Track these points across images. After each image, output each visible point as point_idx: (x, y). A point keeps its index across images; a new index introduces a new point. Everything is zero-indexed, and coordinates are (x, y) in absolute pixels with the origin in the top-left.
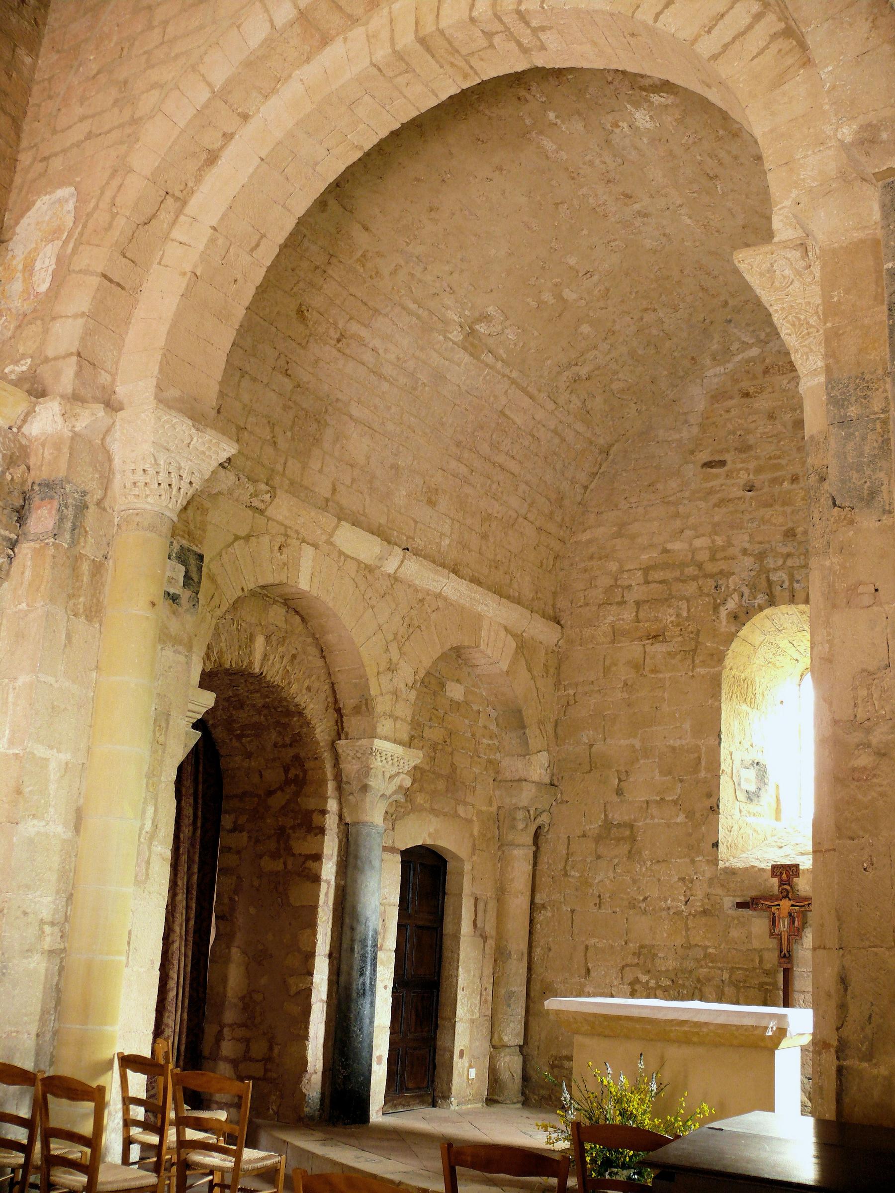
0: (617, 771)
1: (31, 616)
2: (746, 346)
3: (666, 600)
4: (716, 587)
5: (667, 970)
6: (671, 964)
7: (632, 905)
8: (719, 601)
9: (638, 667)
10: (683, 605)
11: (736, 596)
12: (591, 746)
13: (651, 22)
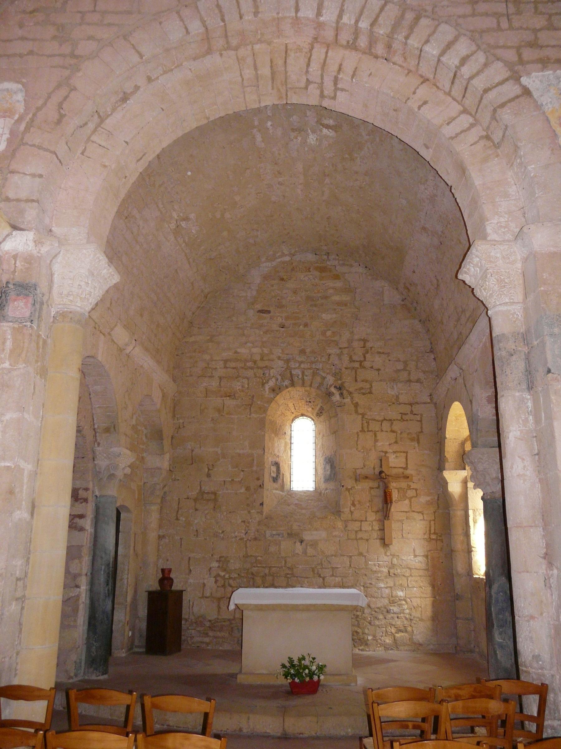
0: (207, 464)
1: (15, 373)
2: (283, 255)
3: (237, 378)
4: (264, 374)
5: (235, 569)
6: (237, 566)
7: (216, 535)
8: (264, 381)
9: (219, 411)
10: (245, 381)
11: (274, 380)
12: (192, 451)
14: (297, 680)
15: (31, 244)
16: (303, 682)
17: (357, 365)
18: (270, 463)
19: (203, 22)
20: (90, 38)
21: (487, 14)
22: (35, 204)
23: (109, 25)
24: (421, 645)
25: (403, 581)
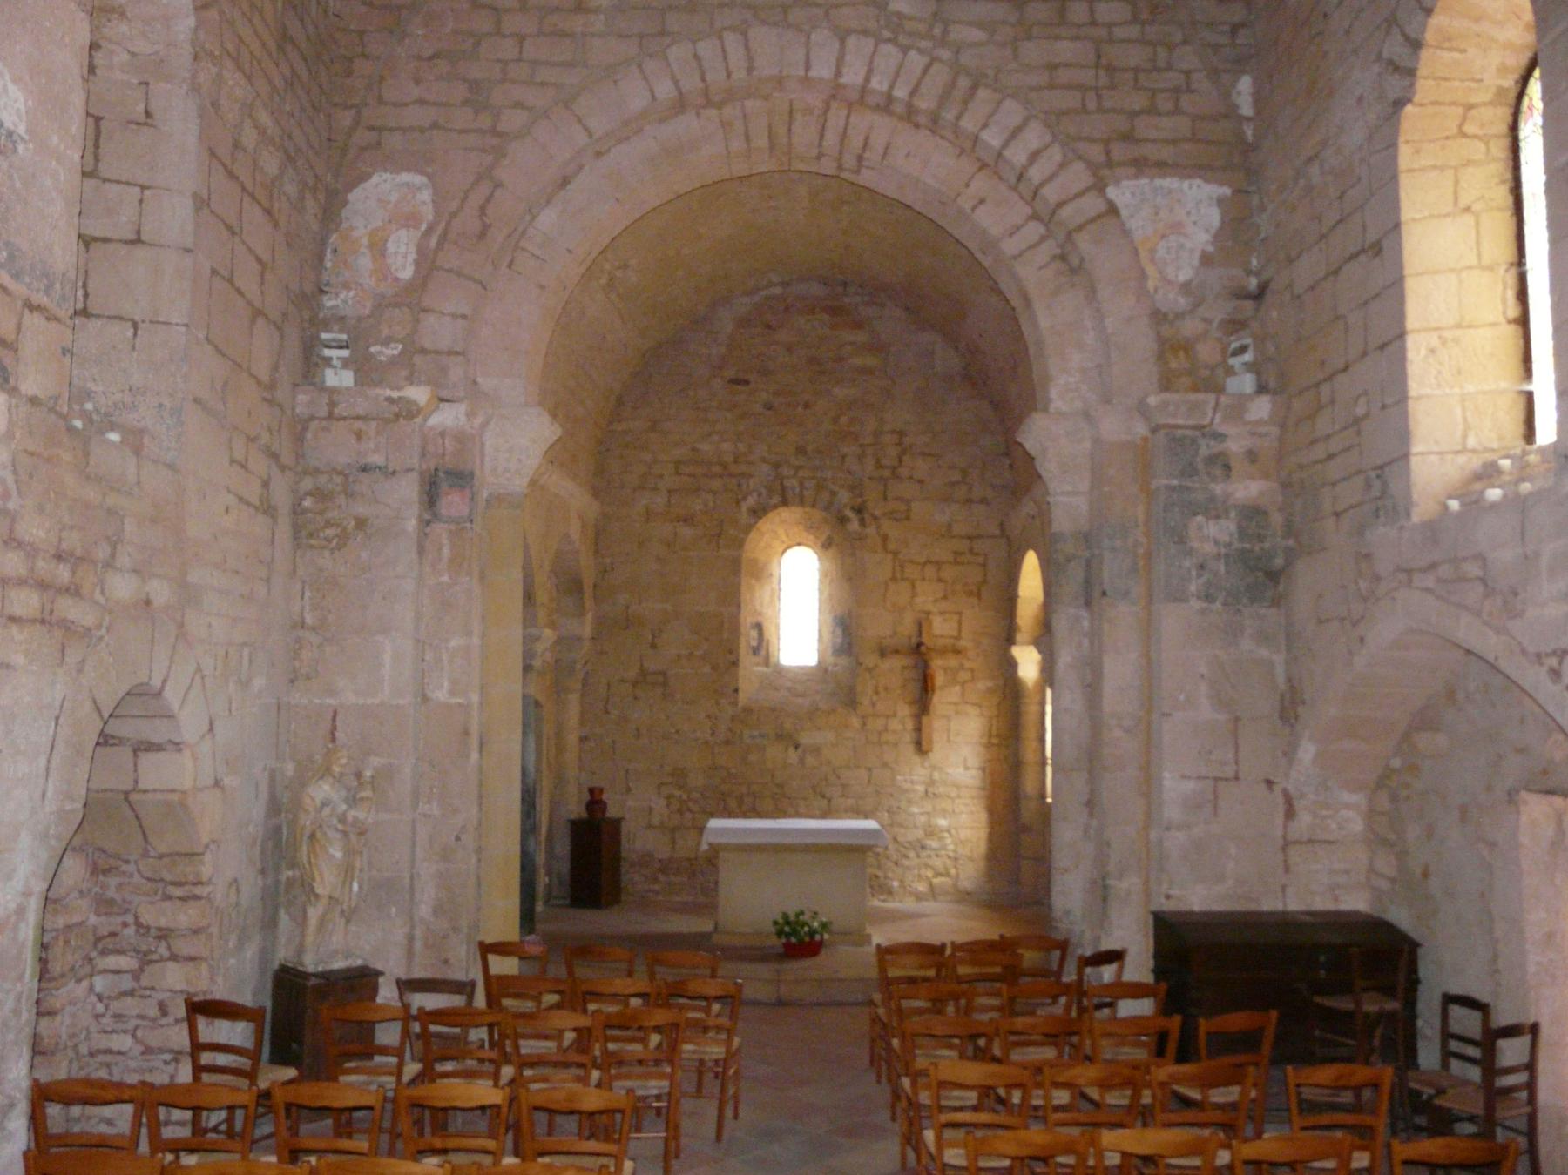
10: (710, 497)
11: (755, 495)
12: (627, 607)
13: (969, 211)
14: (793, 940)
15: (463, 418)
16: (801, 941)
17: (886, 473)
18: (749, 625)
19: (676, 82)
20: (519, 105)
21: (1068, 87)
22: (461, 358)
23: (543, 84)
24: (968, 894)
25: (947, 805)
